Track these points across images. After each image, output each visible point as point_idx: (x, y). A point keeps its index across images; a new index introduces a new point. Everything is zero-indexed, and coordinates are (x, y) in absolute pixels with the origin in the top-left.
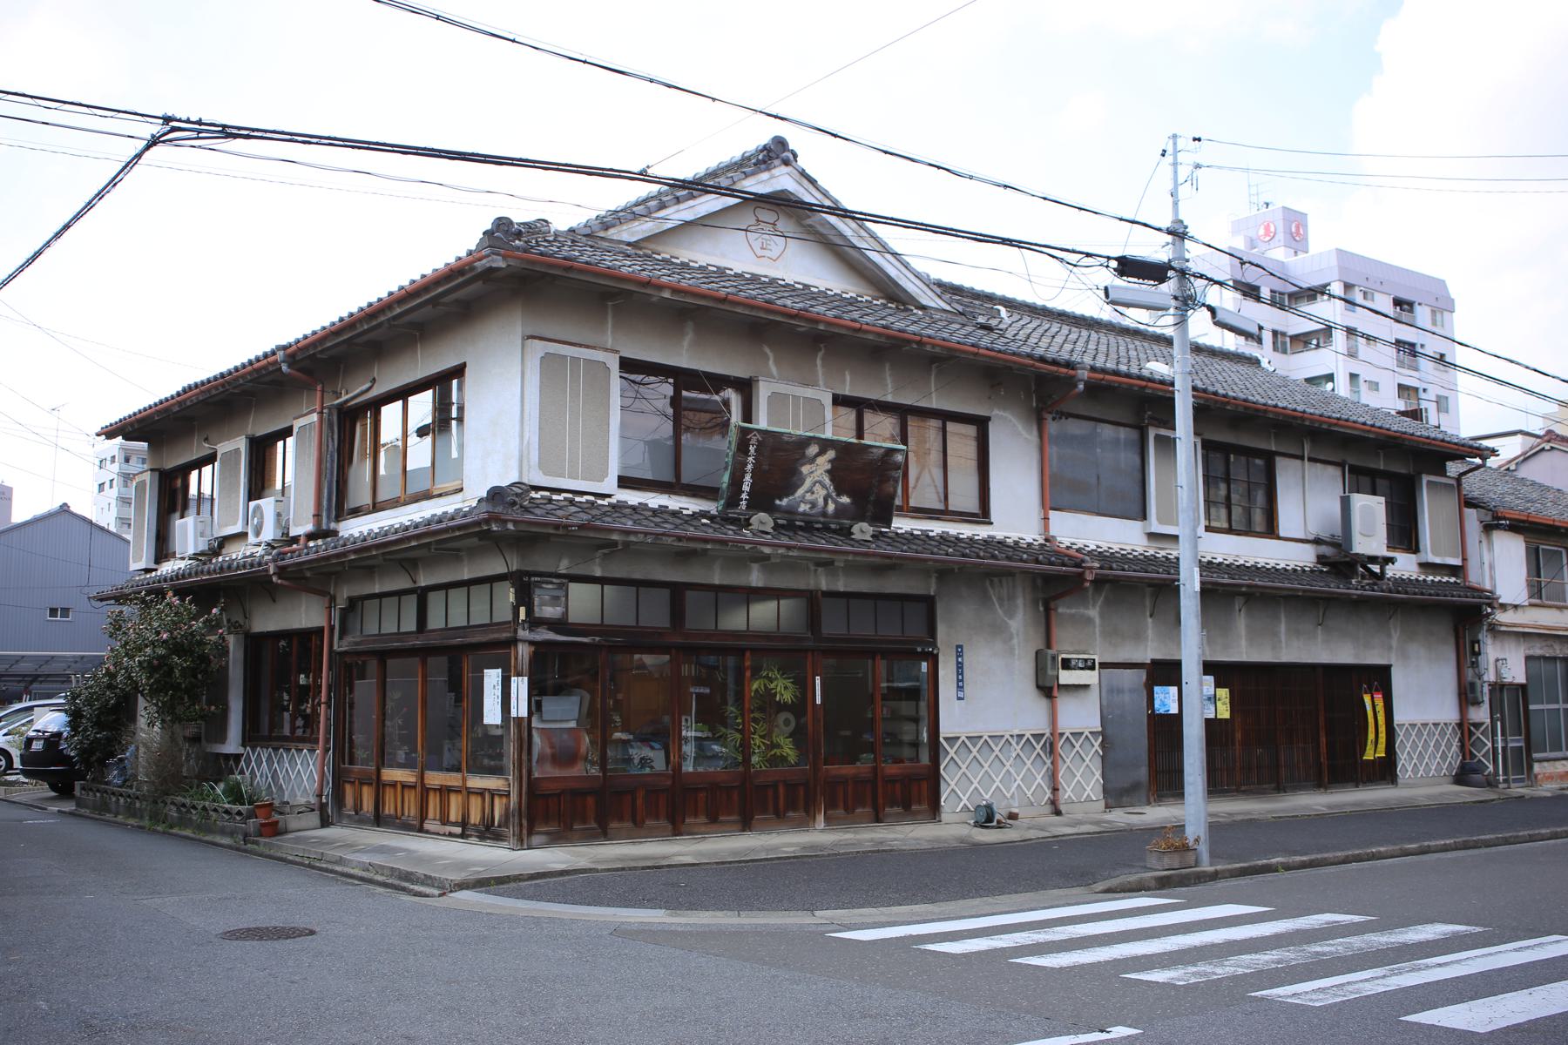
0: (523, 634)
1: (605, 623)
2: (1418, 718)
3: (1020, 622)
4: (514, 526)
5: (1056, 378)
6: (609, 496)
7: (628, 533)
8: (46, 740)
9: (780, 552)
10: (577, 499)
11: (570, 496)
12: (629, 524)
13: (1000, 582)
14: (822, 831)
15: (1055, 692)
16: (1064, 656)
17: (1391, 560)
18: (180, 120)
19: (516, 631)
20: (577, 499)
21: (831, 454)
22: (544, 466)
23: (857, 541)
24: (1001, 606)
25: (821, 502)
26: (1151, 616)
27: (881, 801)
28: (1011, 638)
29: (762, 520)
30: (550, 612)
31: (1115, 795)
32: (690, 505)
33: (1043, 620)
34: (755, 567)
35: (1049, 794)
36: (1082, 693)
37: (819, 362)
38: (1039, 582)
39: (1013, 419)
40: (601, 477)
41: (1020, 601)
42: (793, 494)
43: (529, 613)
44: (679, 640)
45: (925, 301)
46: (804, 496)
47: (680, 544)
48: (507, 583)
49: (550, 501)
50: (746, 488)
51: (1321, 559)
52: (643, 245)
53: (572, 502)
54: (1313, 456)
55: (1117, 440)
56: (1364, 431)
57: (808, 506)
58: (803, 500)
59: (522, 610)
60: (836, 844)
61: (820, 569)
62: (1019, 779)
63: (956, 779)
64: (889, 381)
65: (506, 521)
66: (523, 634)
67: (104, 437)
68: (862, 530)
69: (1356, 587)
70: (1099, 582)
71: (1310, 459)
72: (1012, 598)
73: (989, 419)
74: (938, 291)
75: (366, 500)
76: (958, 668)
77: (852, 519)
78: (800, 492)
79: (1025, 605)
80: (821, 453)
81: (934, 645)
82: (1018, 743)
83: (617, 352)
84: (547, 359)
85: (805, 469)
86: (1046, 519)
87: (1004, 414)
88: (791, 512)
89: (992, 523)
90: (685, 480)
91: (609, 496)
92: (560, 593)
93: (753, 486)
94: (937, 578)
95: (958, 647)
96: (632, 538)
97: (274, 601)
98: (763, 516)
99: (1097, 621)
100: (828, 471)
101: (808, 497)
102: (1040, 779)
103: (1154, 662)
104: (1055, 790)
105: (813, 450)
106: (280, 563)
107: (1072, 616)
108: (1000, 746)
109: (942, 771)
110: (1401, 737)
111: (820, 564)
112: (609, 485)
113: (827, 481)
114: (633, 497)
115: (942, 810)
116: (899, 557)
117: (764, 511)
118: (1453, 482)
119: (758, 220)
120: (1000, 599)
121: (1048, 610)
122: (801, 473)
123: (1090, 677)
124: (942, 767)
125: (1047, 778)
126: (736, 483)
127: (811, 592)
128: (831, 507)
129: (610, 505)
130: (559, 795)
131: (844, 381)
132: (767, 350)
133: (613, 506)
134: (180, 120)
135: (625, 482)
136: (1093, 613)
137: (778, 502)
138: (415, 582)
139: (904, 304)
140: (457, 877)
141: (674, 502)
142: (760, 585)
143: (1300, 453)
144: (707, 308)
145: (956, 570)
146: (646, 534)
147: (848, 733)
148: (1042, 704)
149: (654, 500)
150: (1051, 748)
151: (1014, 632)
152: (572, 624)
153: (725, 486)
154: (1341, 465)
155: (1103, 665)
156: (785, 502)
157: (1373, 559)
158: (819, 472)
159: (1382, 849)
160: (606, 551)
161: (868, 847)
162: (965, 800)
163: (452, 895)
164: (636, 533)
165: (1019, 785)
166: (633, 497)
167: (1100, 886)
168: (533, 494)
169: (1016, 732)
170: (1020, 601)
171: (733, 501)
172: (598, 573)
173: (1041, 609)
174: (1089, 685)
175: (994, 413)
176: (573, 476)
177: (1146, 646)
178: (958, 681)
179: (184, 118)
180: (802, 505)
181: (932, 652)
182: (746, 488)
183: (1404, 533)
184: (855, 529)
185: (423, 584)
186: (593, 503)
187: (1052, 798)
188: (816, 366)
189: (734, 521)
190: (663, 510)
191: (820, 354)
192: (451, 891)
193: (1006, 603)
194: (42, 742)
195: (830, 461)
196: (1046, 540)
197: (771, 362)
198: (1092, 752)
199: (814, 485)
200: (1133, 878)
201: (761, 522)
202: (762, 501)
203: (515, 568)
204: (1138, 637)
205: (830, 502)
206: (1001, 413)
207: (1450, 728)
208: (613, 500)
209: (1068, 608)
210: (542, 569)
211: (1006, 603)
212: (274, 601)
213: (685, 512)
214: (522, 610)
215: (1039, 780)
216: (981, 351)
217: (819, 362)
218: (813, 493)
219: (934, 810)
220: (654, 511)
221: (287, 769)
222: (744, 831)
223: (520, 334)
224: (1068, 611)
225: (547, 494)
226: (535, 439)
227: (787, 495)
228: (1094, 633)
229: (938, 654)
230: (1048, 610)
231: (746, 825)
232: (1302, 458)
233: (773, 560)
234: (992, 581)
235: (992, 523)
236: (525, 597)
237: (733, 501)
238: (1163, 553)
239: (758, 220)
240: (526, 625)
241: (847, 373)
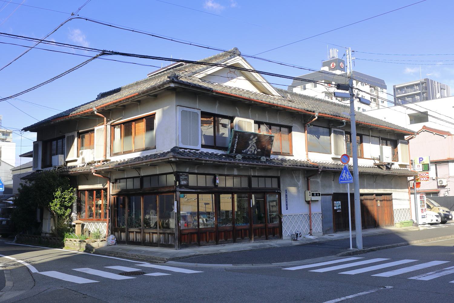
0: (178, 189)
1: (198, 186)
2: (399, 208)
3: (301, 182)
4: (178, 159)
5: (310, 115)
6: (199, 150)
7: (207, 161)
8: (144, 224)
9: (244, 165)
10: (191, 151)
11: (189, 150)
12: (208, 159)
13: (296, 172)
14: (254, 242)
15: (310, 203)
16: (312, 192)
17: (393, 164)
18: (107, 51)
19: (176, 189)
20: (191, 151)
21: (256, 138)
22: (183, 142)
23: (262, 162)
24: (296, 179)
25: (253, 152)
26: (333, 181)
27: (267, 235)
28: (299, 188)
29: (239, 156)
30: (183, 183)
31: (325, 232)
32: (220, 152)
33: (307, 183)
34: (235, 169)
35: (309, 231)
36: (317, 202)
37: (250, 112)
38: (305, 172)
39: (298, 127)
40: (197, 145)
41: (301, 177)
42: (246, 149)
43: (179, 183)
44: (216, 190)
45: (274, 94)
46: (249, 149)
47: (219, 163)
48: (173, 175)
49: (185, 151)
50: (235, 147)
51: (375, 164)
52: (203, 79)
53: (190, 152)
54: (372, 135)
55: (324, 132)
56: (385, 128)
57: (250, 152)
58: (249, 150)
59: (178, 182)
60: (260, 246)
61: (251, 169)
62: (301, 227)
63: (286, 227)
64: (267, 116)
65: (177, 158)
66: (178, 189)
67: (24, 131)
68: (263, 159)
69: (384, 171)
70: (323, 171)
71: (371, 136)
72: (299, 177)
73: (292, 127)
74: (277, 91)
75: (348, 184)
76: (286, 196)
77: (261, 156)
78: (248, 148)
79: (302, 178)
80: (254, 137)
81: (280, 191)
82: (301, 217)
83: (200, 110)
84: (183, 112)
85: (250, 142)
86: (307, 154)
87: (296, 125)
88: (246, 153)
89: (293, 156)
90: (217, 145)
91: (199, 150)
92: (186, 177)
93: (237, 146)
94: (280, 171)
95: (286, 190)
96: (208, 162)
97: (87, 179)
98: (239, 155)
99: (320, 182)
100: (255, 142)
101: (250, 150)
102: (307, 227)
103: (334, 193)
104: (311, 230)
105: (252, 137)
106: (96, 169)
107: (313, 181)
108: (291, 218)
109: (283, 225)
110: (395, 213)
111: (251, 168)
112: (199, 147)
113: (255, 145)
114: (205, 150)
115: (283, 236)
116: (273, 166)
117: (239, 154)
118: (407, 142)
119: (230, 71)
120: (296, 177)
121: (308, 180)
122: (249, 143)
123: (319, 198)
124: (282, 224)
125: (308, 226)
126: (233, 146)
127: (249, 176)
128: (256, 152)
129: (200, 153)
130: (188, 234)
131: (256, 117)
132: (237, 108)
133: (200, 153)
134: (107, 51)
135: (203, 146)
136: (319, 180)
137: (243, 151)
138: (140, 174)
139: (268, 95)
140: (168, 258)
141: (215, 151)
142: (237, 174)
143: (369, 134)
144: (223, 97)
145: (286, 169)
146: (211, 161)
147: (239, 213)
148: (307, 205)
149: (210, 151)
150: (310, 218)
151: (300, 186)
152: (190, 186)
153: (230, 147)
154: (379, 137)
155: (322, 195)
156: (244, 151)
157: (389, 164)
158: (253, 143)
159: (403, 243)
160: (198, 165)
161: (268, 246)
162: (288, 233)
163: (167, 262)
164: (208, 161)
165: (302, 229)
166: (205, 150)
167: (340, 254)
168: (180, 150)
169: (301, 214)
170: (301, 177)
171: (232, 151)
172: (196, 172)
173: (306, 179)
174: (318, 200)
175: (294, 125)
176: (190, 145)
177: (332, 189)
178: (286, 199)
179: (109, 51)
180: (249, 152)
181: (279, 192)
182: (235, 147)
183: (395, 156)
184: (262, 158)
185: (142, 175)
186: (195, 152)
187: (310, 232)
188: (249, 112)
189: (231, 157)
190: (212, 154)
191: (250, 109)
192: (167, 261)
193: (297, 178)
194: (6, 222)
195: (256, 140)
196: (307, 160)
197: (238, 112)
198: (320, 219)
199: (252, 146)
200: (345, 253)
201: (239, 157)
202: (239, 151)
203: (175, 171)
204: (330, 186)
205: (255, 151)
206: (295, 125)
207: (407, 210)
208: (200, 151)
209: (313, 179)
210: (183, 171)
211: (297, 178)
212: (87, 179)
213: (218, 154)
214: (178, 182)
215: (307, 227)
216: (293, 108)
217: (250, 112)
218: (251, 148)
219: (280, 236)
220: (210, 154)
221: (94, 229)
222: (234, 243)
223: (175, 105)
224: (313, 180)
225: (184, 150)
226: (180, 134)
227: (245, 150)
228: (319, 186)
229: (281, 193)
230: (308, 180)
231: (234, 241)
232: (369, 136)
233: (241, 167)
234: (294, 172)
235: (293, 156)
236: (178, 179)
237: (232, 151)
238: (336, 163)
239: (230, 71)
240: (179, 187)
241: (257, 115)
